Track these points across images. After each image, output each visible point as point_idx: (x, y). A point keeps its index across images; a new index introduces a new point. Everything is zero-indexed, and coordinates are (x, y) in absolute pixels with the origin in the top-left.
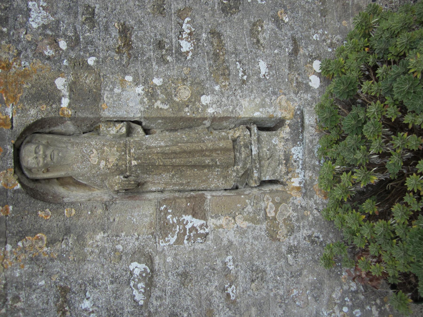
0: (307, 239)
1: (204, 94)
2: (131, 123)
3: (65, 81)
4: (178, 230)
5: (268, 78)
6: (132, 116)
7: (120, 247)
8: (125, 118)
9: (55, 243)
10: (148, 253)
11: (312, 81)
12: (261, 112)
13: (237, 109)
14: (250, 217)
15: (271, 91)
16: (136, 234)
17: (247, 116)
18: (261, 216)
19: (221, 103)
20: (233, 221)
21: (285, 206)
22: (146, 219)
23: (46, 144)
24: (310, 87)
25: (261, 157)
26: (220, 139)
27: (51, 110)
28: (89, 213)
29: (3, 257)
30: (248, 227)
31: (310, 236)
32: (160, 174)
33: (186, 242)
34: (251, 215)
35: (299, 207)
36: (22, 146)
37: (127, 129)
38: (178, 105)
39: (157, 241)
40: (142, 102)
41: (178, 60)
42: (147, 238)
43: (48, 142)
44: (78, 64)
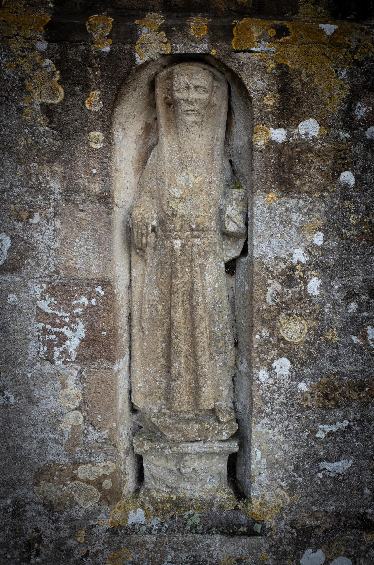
0: (35, 535)
1: (292, 363)
2: (245, 239)
3: (313, 136)
4: (60, 315)
5: (320, 475)
6: (254, 243)
7: (36, 218)
8: (252, 231)
9: (47, 116)
10: (24, 265)
11: (314, 554)
12: (259, 462)
13: (266, 420)
14: (79, 436)
15: (296, 481)
16: (58, 245)
17: (253, 437)
18: (79, 455)
19: (275, 392)
20: (73, 407)
21: (94, 497)
22: (80, 261)
23: (211, 103)
24: (303, 550)
25: (183, 458)
26: (216, 387)
27: (265, 112)
28: (95, 171)
29: (28, 37)
30: (61, 433)
31: (39, 540)
32: (158, 286)
33: (41, 326)
34: (82, 438)
35: (92, 522)
36: (206, 67)
37: (233, 232)
38: (273, 320)
39: (44, 280)
40: (278, 259)
41: (353, 320)
42: (49, 263)
43: (214, 105)
44: (343, 156)
